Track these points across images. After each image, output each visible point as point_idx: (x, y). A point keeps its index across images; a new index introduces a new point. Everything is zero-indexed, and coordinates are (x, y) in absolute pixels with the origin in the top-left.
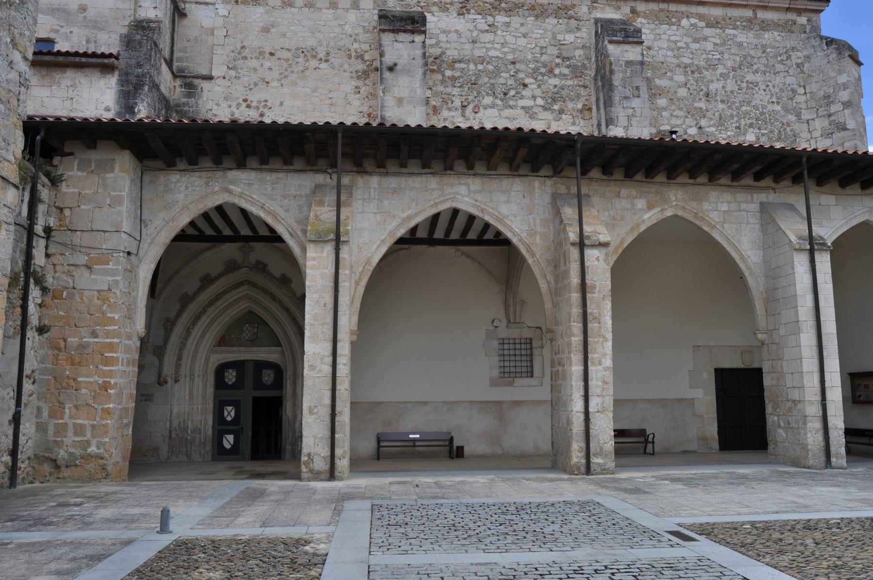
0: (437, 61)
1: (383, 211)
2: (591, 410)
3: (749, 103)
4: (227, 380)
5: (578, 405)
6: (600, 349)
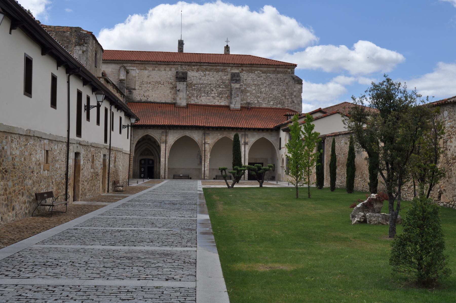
1: (172, 138)
3: (272, 94)
5: (203, 169)
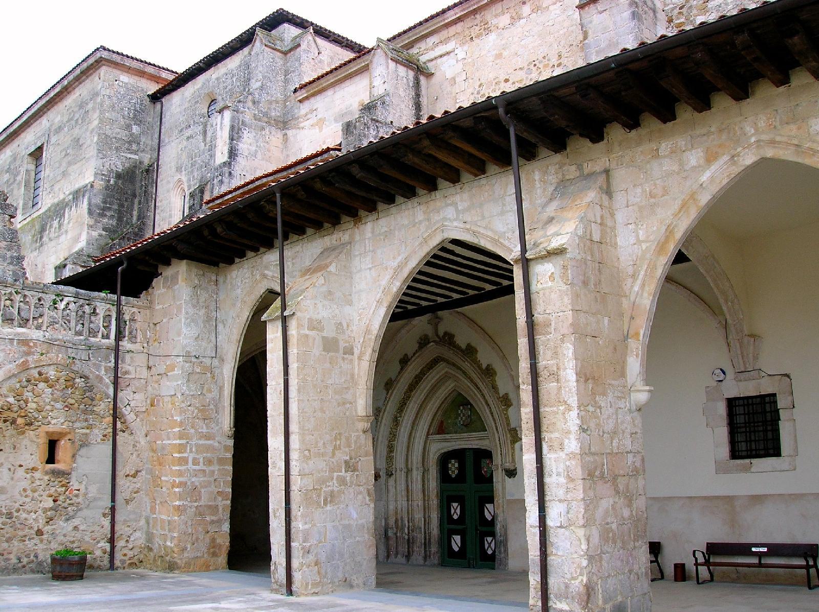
0: (684, 10)
2: (550, 522)
4: (450, 472)
6: (560, 425)
